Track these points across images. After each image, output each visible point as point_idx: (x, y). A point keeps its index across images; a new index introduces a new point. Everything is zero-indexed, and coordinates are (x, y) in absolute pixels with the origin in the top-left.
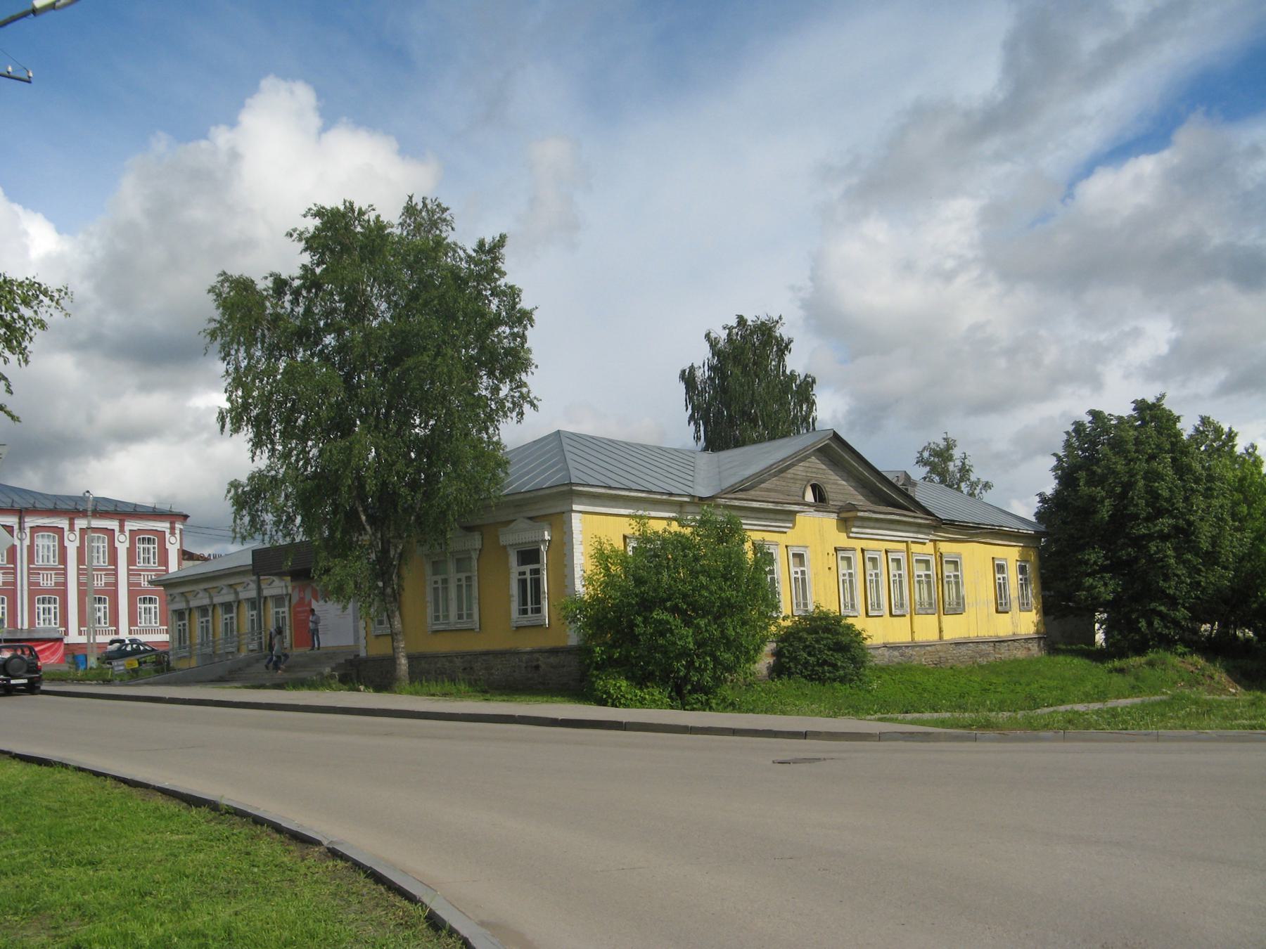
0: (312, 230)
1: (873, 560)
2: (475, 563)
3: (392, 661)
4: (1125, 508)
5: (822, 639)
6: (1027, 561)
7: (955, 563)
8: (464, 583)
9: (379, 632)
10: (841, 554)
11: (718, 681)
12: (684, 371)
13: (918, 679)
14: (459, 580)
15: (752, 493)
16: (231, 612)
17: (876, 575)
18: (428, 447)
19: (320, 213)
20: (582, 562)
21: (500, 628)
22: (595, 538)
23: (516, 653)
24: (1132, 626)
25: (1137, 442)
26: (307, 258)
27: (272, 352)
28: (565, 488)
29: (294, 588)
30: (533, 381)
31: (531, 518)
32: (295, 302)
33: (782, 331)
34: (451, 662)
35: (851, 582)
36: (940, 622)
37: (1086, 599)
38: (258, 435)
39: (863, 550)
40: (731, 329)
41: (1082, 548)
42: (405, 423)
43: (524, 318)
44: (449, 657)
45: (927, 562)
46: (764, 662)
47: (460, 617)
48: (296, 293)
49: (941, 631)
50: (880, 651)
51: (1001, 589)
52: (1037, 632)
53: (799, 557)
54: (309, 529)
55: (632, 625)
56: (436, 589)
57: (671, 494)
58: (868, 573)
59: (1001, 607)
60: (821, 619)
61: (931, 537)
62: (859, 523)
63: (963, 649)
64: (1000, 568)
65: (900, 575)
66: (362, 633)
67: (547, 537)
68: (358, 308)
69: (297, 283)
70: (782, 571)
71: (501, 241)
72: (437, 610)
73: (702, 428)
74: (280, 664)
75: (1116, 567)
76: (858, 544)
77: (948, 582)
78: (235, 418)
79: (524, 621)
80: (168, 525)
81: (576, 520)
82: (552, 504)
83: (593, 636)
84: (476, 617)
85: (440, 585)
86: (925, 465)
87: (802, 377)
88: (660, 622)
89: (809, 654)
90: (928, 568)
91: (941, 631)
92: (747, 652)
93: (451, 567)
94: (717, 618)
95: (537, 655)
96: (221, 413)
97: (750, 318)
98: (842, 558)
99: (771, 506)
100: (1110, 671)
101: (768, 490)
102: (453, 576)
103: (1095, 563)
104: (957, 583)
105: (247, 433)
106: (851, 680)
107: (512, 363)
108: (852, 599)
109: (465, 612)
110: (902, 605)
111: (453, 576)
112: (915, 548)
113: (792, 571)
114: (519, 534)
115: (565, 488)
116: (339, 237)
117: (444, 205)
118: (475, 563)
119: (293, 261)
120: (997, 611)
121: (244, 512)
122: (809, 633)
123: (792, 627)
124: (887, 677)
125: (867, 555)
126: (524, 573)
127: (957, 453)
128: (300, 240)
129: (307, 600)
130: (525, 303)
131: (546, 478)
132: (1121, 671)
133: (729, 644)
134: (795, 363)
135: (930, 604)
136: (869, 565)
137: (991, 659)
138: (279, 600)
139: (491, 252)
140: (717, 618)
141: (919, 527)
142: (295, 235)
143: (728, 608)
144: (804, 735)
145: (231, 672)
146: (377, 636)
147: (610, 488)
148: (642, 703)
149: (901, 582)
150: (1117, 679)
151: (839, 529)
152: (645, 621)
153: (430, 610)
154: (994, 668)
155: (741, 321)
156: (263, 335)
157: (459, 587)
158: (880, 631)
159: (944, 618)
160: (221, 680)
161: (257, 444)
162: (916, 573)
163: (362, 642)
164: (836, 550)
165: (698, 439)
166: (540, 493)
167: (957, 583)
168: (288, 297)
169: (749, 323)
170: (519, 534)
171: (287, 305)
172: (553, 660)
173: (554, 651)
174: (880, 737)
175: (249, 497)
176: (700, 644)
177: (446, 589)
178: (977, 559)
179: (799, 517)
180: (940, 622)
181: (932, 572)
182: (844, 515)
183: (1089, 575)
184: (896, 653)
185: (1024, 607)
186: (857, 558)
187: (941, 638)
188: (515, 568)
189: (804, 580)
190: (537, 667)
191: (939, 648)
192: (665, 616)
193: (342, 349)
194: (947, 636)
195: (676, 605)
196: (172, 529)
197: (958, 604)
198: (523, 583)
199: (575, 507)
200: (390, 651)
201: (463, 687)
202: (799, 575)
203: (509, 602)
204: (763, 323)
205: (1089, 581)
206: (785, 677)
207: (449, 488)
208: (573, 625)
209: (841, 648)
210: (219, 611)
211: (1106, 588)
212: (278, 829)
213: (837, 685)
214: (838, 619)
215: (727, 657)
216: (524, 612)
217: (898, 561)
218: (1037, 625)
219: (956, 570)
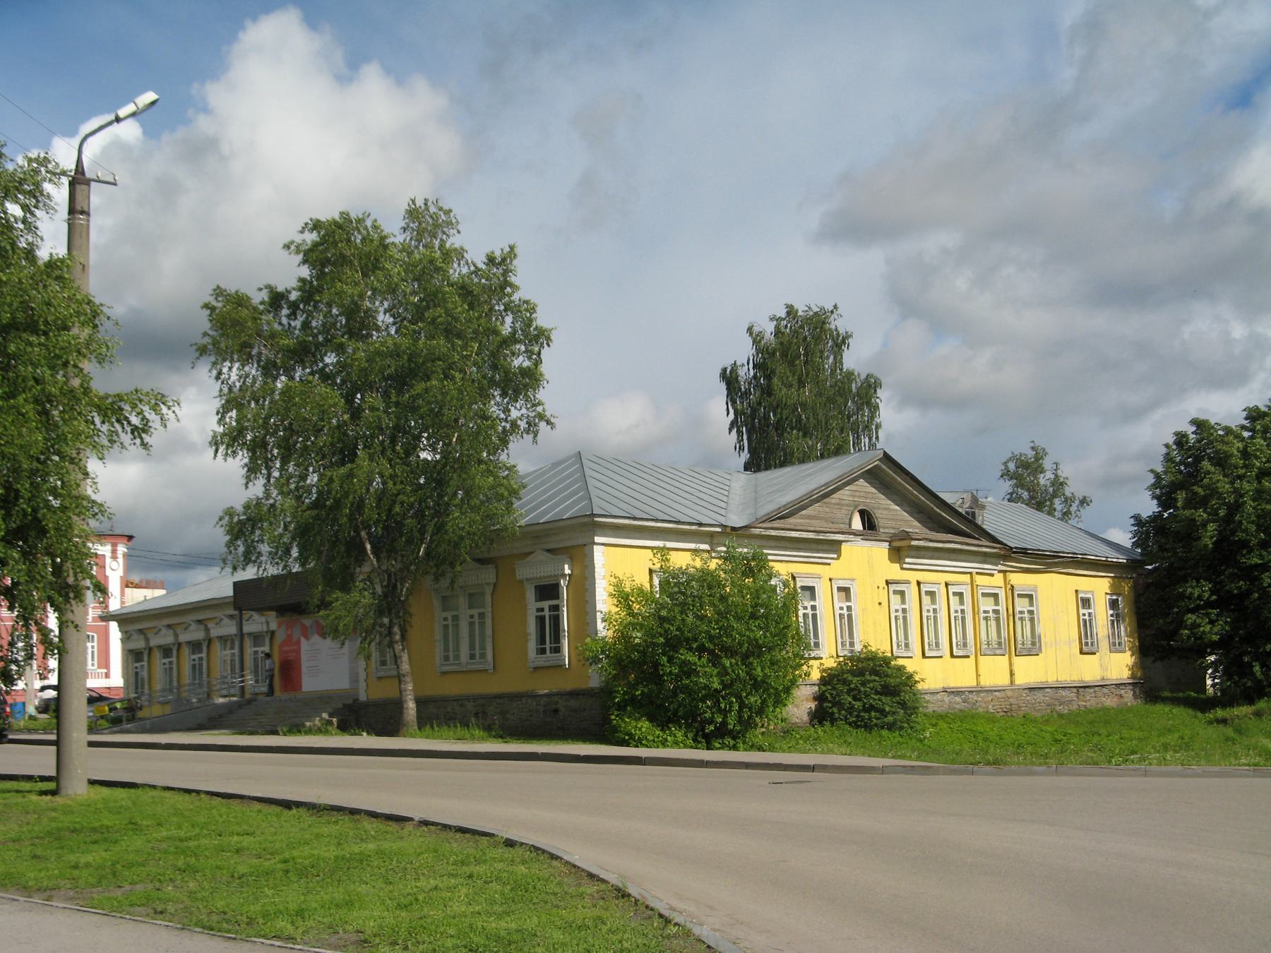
0: (309, 242)
1: (932, 594)
2: (488, 599)
3: (399, 704)
4: (1233, 533)
5: (869, 681)
6: (1118, 595)
7: (1030, 597)
8: (476, 619)
9: (382, 674)
10: (892, 587)
11: (747, 725)
12: (725, 370)
13: (980, 728)
14: (472, 617)
15: (792, 521)
16: (201, 652)
17: (935, 610)
18: (438, 475)
19: (316, 225)
20: (604, 602)
21: (517, 672)
22: (620, 569)
23: (535, 696)
24: (1245, 670)
25: (1245, 454)
26: (305, 272)
27: (269, 370)
28: (586, 519)
29: (279, 626)
30: (546, 395)
31: (549, 551)
32: (292, 316)
33: (840, 324)
34: (462, 706)
35: (905, 619)
36: (1011, 664)
37: (1189, 637)
38: (253, 459)
39: (919, 583)
40: (779, 319)
41: (1184, 579)
42: (412, 449)
43: (540, 337)
44: (459, 700)
45: (996, 596)
46: (800, 705)
47: (472, 657)
48: (294, 307)
49: (1012, 674)
50: (939, 697)
51: (1086, 627)
52: (1133, 676)
53: (845, 591)
54: (303, 560)
55: (656, 665)
56: (446, 627)
57: (700, 525)
58: (925, 608)
59: (1087, 647)
60: (867, 659)
61: (1000, 567)
62: (913, 553)
63: (1039, 695)
64: (1086, 603)
65: (963, 611)
66: (362, 675)
67: (567, 571)
68: (359, 324)
69: (294, 296)
70: (826, 605)
71: (512, 252)
72: (446, 649)
73: (745, 437)
74: (273, 705)
75: (1224, 602)
76: (913, 576)
77: (1021, 619)
78: (230, 440)
79: (542, 661)
80: (109, 547)
81: (598, 552)
82: (573, 537)
83: (615, 677)
84: (490, 657)
85: (450, 622)
86: (1011, 479)
87: (863, 377)
88: (685, 663)
89: (855, 699)
90: (997, 603)
91: (1012, 674)
92: (777, 694)
93: (462, 601)
94: (745, 657)
95: (557, 699)
96: (214, 437)
97: (801, 309)
98: (895, 592)
99: (811, 535)
100: (1210, 723)
101: (809, 517)
102: (465, 613)
103: (1200, 597)
104: (1032, 620)
105: (242, 458)
106: (901, 728)
107: (523, 384)
108: (906, 637)
109: (477, 652)
110: (965, 645)
111: (465, 613)
112: (980, 580)
113: (837, 606)
114: (537, 568)
115: (586, 519)
116: (337, 249)
117: (446, 207)
118: (488, 599)
119: (290, 274)
120: (1082, 653)
121: (239, 542)
122: (854, 675)
123: (835, 669)
124: (945, 725)
125: (924, 588)
126: (542, 610)
127: (1047, 463)
128: (298, 252)
129: (295, 639)
130: (542, 319)
131: (567, 509)
132: (1223, 721)
133: (757, 685)
134: (855, 359)
135: (1000, 644)
136: (926, 600)
137: (1074, 707)
138: (257, 638)
139: (501, 263)
140: (745, 657)
141: (985, 558)
142: (293, 247)
143: (756, 649)
144: (812, 768)
145: (210, 719)
146: (380, 678)
147: (635, 519)
148: (664, 743)
149: (963, 619)
150: (1214, 732)
151: (892, 559)
152: (670, 660)
153: (439, 650)
154: (1072, 718)
155: (791, 311)
156: (260, 353)
157: (472, 624)
158: (935, 674)
159: (1016, 660)
160: (200, 727)
161: (252, 470)
162: (982, 609)
163: (362, 685)
164: (887, 583)
165: (741, 448)
166: (561, 524)
167: (1032, 620)
168: (285, 312)
169: (800, 313)
170: (537, 568)
171: (285, 321)
172: (573, 703)
173: (574, 694)
174: (883, 770)
175: (244, 527)
176: (725, 687)
177: (456, 626)
178: (1056, 595)
179: (844, 546)
180: (1011, 664)
181: (1002, 608)
182: (896, 544)
183: (1192, 611)
184: (958, 699)
185: (1115, 647)
186: (912, 592)
187: (1012, 682)
188: (532, 604)
189: (850, 617)
190: (556, 711)
191: (1009, 694)
192: (692, 658)
193: (342, 366)
194: (1020, 680)
195: (703, 645)
196: (114, 552)
197: (1033, 644)
198: (541, 620)
199: (597, 539)
200: (397, 695)
201: (477, 732)
202: (845, 612)
203: (527, 641)
204: (816, 313)
205: (1191, 618)
206: (827, 724)
207: (458, 520)
208: (593, 667)
209: (888, 691)
210: (186, 651)
211: (1212, 629)
212: (373, 815)
213: (885, 733)
214: (886, 661)
215: (754, 700)
216: (543, 651)
217: (960, 595)
218: (1131, 669)
219: (1031, 604)
